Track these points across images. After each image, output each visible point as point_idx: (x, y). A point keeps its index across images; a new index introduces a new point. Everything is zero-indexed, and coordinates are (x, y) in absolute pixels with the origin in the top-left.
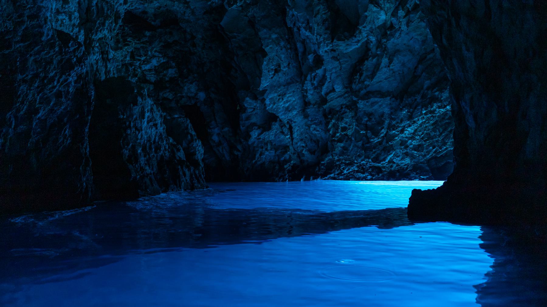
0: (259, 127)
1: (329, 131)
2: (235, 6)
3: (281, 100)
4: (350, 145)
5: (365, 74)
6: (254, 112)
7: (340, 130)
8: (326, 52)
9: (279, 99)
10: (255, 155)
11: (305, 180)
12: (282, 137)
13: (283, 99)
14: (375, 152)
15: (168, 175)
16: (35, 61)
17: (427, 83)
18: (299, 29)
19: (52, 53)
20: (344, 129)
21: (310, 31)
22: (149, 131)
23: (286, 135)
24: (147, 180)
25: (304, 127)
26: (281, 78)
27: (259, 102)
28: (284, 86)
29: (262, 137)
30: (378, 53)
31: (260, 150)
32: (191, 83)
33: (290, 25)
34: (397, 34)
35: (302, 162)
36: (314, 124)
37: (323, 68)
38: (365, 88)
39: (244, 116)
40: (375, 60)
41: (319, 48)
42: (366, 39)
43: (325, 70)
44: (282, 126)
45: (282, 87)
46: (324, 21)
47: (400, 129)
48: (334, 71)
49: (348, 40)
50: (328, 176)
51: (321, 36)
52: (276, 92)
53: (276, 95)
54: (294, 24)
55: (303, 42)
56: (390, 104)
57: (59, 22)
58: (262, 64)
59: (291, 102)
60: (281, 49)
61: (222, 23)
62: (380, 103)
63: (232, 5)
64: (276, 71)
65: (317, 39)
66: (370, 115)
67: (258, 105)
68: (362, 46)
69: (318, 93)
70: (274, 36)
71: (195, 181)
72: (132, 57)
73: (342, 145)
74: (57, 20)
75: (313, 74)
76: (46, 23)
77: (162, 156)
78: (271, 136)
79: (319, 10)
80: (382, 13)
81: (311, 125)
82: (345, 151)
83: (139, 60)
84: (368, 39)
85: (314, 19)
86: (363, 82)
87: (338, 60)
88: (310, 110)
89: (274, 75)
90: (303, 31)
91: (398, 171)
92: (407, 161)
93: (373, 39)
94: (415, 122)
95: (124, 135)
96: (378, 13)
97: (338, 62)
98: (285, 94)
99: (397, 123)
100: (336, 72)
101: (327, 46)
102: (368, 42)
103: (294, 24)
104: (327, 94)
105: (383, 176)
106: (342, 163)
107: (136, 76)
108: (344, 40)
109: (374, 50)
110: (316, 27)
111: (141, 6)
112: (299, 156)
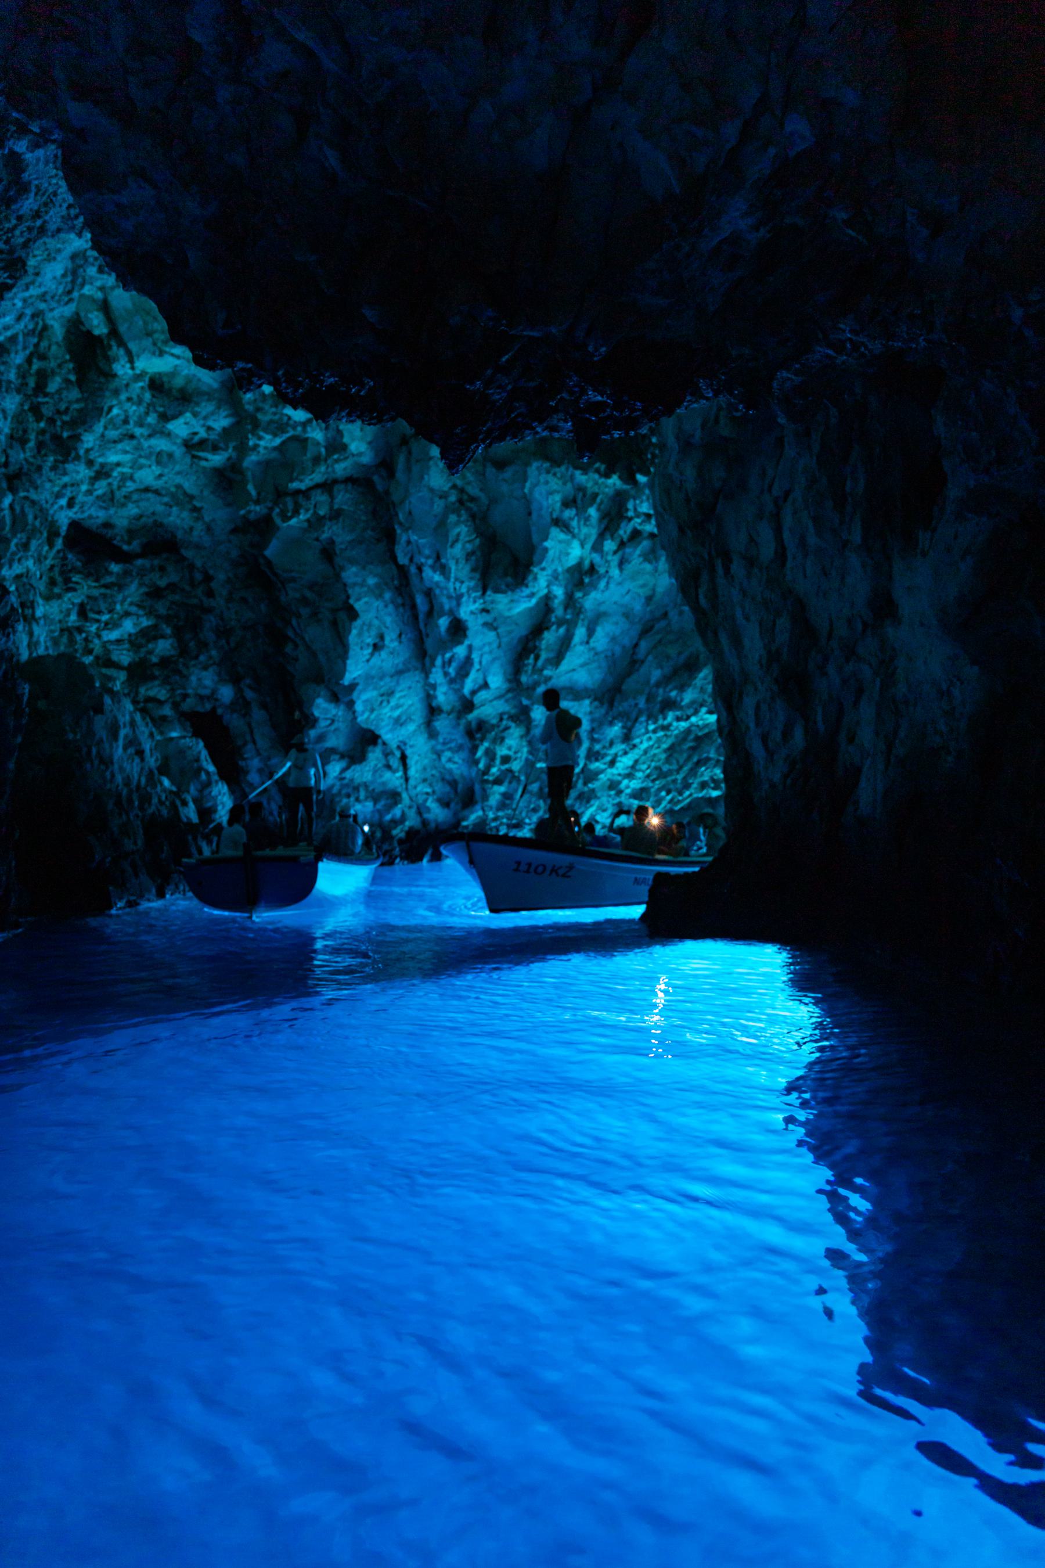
0: (342, 756)
3: (384, 704)
5: (544, 656)
6: (333, 728)
7: (498, 761)
8: (472, 613)
9: (382, 702)
11: (431, 860)
12: (388, 775)
13: (388, 702)
17: (656, 674)
18: (420, 569)
20: (506, 759)
22: (127, 766)
23: (395, 771)
26: (385, 661)
27: (342, 707)
28: (392, 676)
29: (348, 775)
30: (568, 617)
32: (205, 668)
33: (403, 560)
34: (602, 584)
35: (425, 823)
36: (450, 749)
37: (467, 642)
39: (313, 733)
40: (562, 630)
41: (459, 604)
42: (545, 591)
43: (470, 648)
44: (387, 754)
45: (387, 679)
46: (468, 556)
47: (608, 759)
51: (462, 582)
52: (375, 688)
53: (375, 693)
54: (411, 560)
56: (591, 713)
58: (350, 632)
59: (405, 707)
60: (386, 606)
61: (268, 553)
63: (290, 518)
64: (376, 647)
65: (455, 589)
67: (340, 713)
68: (537, 604)
70: (371, 581)
72: (82, 612)
73: (502, 789)
75: (448, 655)
78: (365, 774)
79: (459, 535)
80: (576, 544)
81: (443, 751)
82: (508, 802)
83: (98, 621)
86: (542, 670)
87: (495, 629)
88: (442, 724)
89: (372, 654)
90: (428, 572)
93: (559, 592)
94: (635, 746)
96: (568, 543)
99: (604, 747)
100: (491, 652)
101: (475, 602)
102: (548, 598)
104: (474, 692)
106: (502, 824)
108: (504, 592)
109: (559, 612)
112: (419, 813)
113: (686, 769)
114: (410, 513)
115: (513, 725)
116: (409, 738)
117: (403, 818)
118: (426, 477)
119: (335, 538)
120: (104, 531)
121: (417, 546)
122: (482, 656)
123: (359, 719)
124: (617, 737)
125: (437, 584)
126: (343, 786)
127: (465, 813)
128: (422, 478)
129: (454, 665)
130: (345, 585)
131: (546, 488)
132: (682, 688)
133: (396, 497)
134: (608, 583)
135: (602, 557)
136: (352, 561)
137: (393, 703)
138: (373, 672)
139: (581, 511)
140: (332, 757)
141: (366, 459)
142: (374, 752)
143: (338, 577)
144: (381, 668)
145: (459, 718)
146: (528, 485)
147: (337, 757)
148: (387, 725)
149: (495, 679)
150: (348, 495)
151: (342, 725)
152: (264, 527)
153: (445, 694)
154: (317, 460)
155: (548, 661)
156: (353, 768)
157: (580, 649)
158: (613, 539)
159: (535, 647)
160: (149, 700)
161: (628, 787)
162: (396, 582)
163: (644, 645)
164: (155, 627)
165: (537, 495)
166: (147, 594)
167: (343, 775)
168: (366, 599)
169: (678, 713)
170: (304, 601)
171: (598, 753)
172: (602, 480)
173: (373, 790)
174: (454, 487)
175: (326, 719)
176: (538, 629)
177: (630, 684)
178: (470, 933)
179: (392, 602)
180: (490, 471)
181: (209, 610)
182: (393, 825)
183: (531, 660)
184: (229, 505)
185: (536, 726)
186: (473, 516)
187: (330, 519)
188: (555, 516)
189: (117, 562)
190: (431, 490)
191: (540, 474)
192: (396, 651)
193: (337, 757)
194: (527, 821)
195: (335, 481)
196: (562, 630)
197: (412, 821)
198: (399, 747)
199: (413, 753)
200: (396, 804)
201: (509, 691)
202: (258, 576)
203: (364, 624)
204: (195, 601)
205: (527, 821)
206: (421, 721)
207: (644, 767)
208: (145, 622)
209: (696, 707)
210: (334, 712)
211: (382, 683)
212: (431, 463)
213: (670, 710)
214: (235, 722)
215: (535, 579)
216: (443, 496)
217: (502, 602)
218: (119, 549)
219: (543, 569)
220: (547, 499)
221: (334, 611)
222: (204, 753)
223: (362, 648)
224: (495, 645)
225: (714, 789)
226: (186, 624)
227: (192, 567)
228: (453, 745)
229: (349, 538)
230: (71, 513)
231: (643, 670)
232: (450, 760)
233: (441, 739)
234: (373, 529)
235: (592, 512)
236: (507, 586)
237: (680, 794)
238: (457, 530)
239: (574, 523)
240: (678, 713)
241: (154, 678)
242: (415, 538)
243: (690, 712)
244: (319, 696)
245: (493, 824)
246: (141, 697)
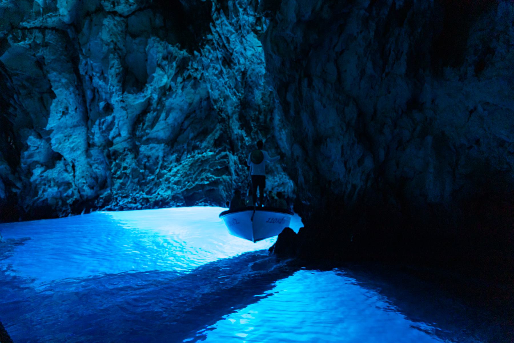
0: (42, 165)
2: (22, 42)
3: (67, 141)
4: (127, 182)
5: (147, 124)
6: (37, 151)
7: (122, 169)
8: (117, 101)
9: (65, 140)
10: (38, 192)
11: (85, 213)
12: (66, 175)
13: (69, 140)
14: (148, 187)
17: (191, 135)
18: (91, 78)
20: (125, 168)
23: (69, 173)
25: (86, 165)
27: (43, 141)
28: (71, 128)
29: (45, 174)
30: (158, 108)
31: (43, 187)
33: (82, 72)
34: (174, 96)
35: (81, 196)
36: (97, 163)
37: (113, 115)
39: (26, 153)
40: (155, 114)
41: (111, 97)
43: (114, 118)
44: (66, 165)
46: (117, 75)
47: (169, 168)
48: (122, 118)
49: (136, 94)
50: (106, 207)
51: (114, 86)
52: (62, 133)
53: (62, 135)
54: (86, 73)
56: (164, 149)
58: (51, 104)
59: (77, 143)
60: (70, 94)
62: (157, 148)
63: (20, 41)
64: (64, 113)
65: (110, 89)
66: (149, 157)
68: (145, 101)
70: (64, 81)
73: (121, 181)
75: (103, 120)
78: (54, 174)
79: (114, 64)
80: (166, 77)
81: (94, 164)
82: (123, 187)
84: (151, 96)
85: (109, 70)
87: (126, 110)
88: (94, 152)
89: (62, 116)
91: (161, 200)
92: (169, 192)
93: (156, 96)
94: (181, 164)
96: (163, 76)
98: (71, 136)
99: (168, 164)
100: (123, 120)
101: (119, 96)
102: (150, 100)
104: (114, 138)
105: (150, 205)
106: (119, 196)
108: (133, 94)
109: (155, 105)
112: (79, 192)
113: (197, 173)
114: (89, 50)
115: (129, 153)
116: (77, 157)
118: (100, 33)
119: (45, 57)
121: (92, 66)
122: (119, 121)
123: (53, 148)
124: (173, 160)
125: (100, 86)
126: (42, 180)
127: (102, 191)
128: (98, 34)
129: (105, 124)
130: (49, 81)
131: (156, 49)
132: (201, 141)
134: (176, 95)
135: (176, 84)
136: (54, 70)
137: (71, 140)
138: (62, 125)
139: (170, 62)
140: (37, 166)
141: (66, 19)
142: (59, 163)
143: (45, 76)
144: (66, 123)
146: (148, 47)
147: (39, 165)
148: (67, 151)
149: (124, 132)
150: (53, 36)
151: (43, 150)
153: (98, 138)
154: (38, 14)
156: (48, 171)
157: (163, 122)
158: (181, 77)
159: (143, 120)
161: (173, 180)
162: (76, 83)
163: (186, 123)
165: (151, 52)
167: (43, 175)
168: (60, 89)
169: (199, 151)
170: (24, 87)
171: (166, 166)
172: (179, 51)
173: (58, 182)
174: (112, 41)
175: (35, 147)
177: (181, 138)
178: (209, 272)
179: (74, 92)
180: (129, 38)
182: (67, 198)
183: (141, 125)
185: (141, 154)
186: (120, 57)
187: (43, 46)
188: (159, 63)
190: (102, 40)
191: (154, 43)
192: (73, 117)
193: (39, 165)
194: (131, 195)
195: (46, 28)
196: (155, 114)
198: (72, 162)
199: (78, 164)
200: (69, 188)
201: (129, 138)
203: (59, 101)
205: (131, 195)
206: (84, 150)
207: (181, 172)
209: (206, 149)
210: (39, 143)
211: (66, 131)
212: (103, 27)
213: (196, 149)
215: (147, 90)
216: (108, 44)
219: (151, 86)
220: (157, 54)
223: (57, 113)
224: (125, 117)
225: (207, 181)
228: (99, 161)
229: (52, 58)
231: (185, 133)
232: (96, 168)
233: (93, 159)
234: (65, 56)
235: (174, 64)
236: (134, 91)
237: (194, 183)
238: (113, 62)
239: (166, 68)
240: (199, 151)
242: (92, 62)
243: (203, 151)
244: (31, 135)
245: (115, 196)
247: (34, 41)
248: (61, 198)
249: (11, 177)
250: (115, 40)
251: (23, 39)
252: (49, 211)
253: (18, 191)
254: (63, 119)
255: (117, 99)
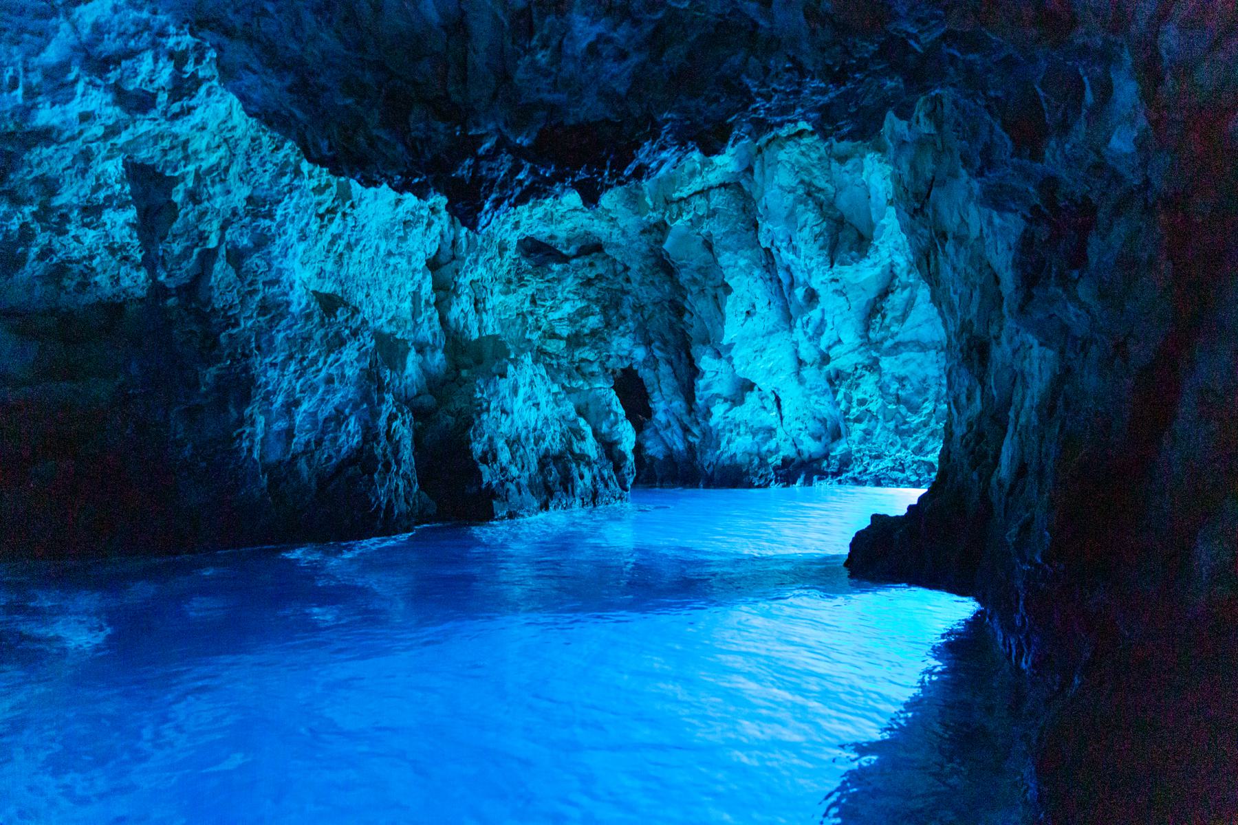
0: (726, 400)
1: (838, 404)
5: (890, 315)
7: (854, 404)
8: (822, 283)
12: (764, 414)
14: (916, 439)
15: (555, 478)
16: (287, 338)
19: (309, 326)
20: (862, 402)
21: (795, 253)
22: (526, 414)
23: (769, 412)
24: (512, 487)
27: (724, 362)
29: (730, 414)
30: (911, 281)
31: (728, 435)
32: (623, 336)
35: (799, 453)
37: (819, 307)
38: (892, 337)
40: (906, 293)
41: (810, 277)
42: (889, 260)
43: (823, 310)
51: (811, 259)
52: (749, 346)
53: (750, 350)
54: (772, 243)
55: (788, 269)
57: (391, 268)
61: (665, 246)
66: (901, 380)
68: (883, 272)
69: (816, 346)
71: (601, 486)
72: (533, 302)
74: (388, 266)
75: (805, 319)
76: (292, 287)
77: (547, 450)
88: (807, 373)
89: (746, 320)
90: (784, 253)
95: (477, 422)
97: (843, 299)
103: (772, 243)
104: (829, 348)
107: (539, 328)
108: (850, 264)
110: (801, 245)
111: (546, 229)
117: (777, 450)
120: (549, 242)
125: (792, 261)
127: (834, 445)
129: (811, 325)
131: (135, 280)
133: (755, 196)
136: (726, 249)
143: (716, 261)
145: (820, 368)
146: (865, 173)
152: (661, 228)
155: (895, 319)
160: (583, 360)
164: (588, 306)
166: (582, 284)
170: (694, 281)
174: (802, 182)
176: (885, 293)
180: (835, 165)
181: (628, 293)
184: (636, 214)
186: (820, 205)
187: (708, 217)
189: (558, 262)
190: (781, 187)
192: (768, 315)
195: (711, 188)
196: (906, 293)
197: (787, 451)
202: (664, 266)
204: (617, 286)
208: (580, 304)
214: (646, 374)
215: (877, 250)
216: (792, 191)
217: (848, 273)
218: (560, 252)
221: (715, 287)
222: (616, 400)
224: (845, 308)
226: (611, 305)
227: (614, 261)
229: (723, 230)
230: (518, 233)
236: (853, 259)
241: (585, 345)
246: (576, 358)
247: (695, 215)
248: (759, 454)
249: (686, 419)
250: (806, 179)
251: (680, 215)
252: (734, 477)
253: (697, 441)
254: (749, 323)
255: (822, 278)
